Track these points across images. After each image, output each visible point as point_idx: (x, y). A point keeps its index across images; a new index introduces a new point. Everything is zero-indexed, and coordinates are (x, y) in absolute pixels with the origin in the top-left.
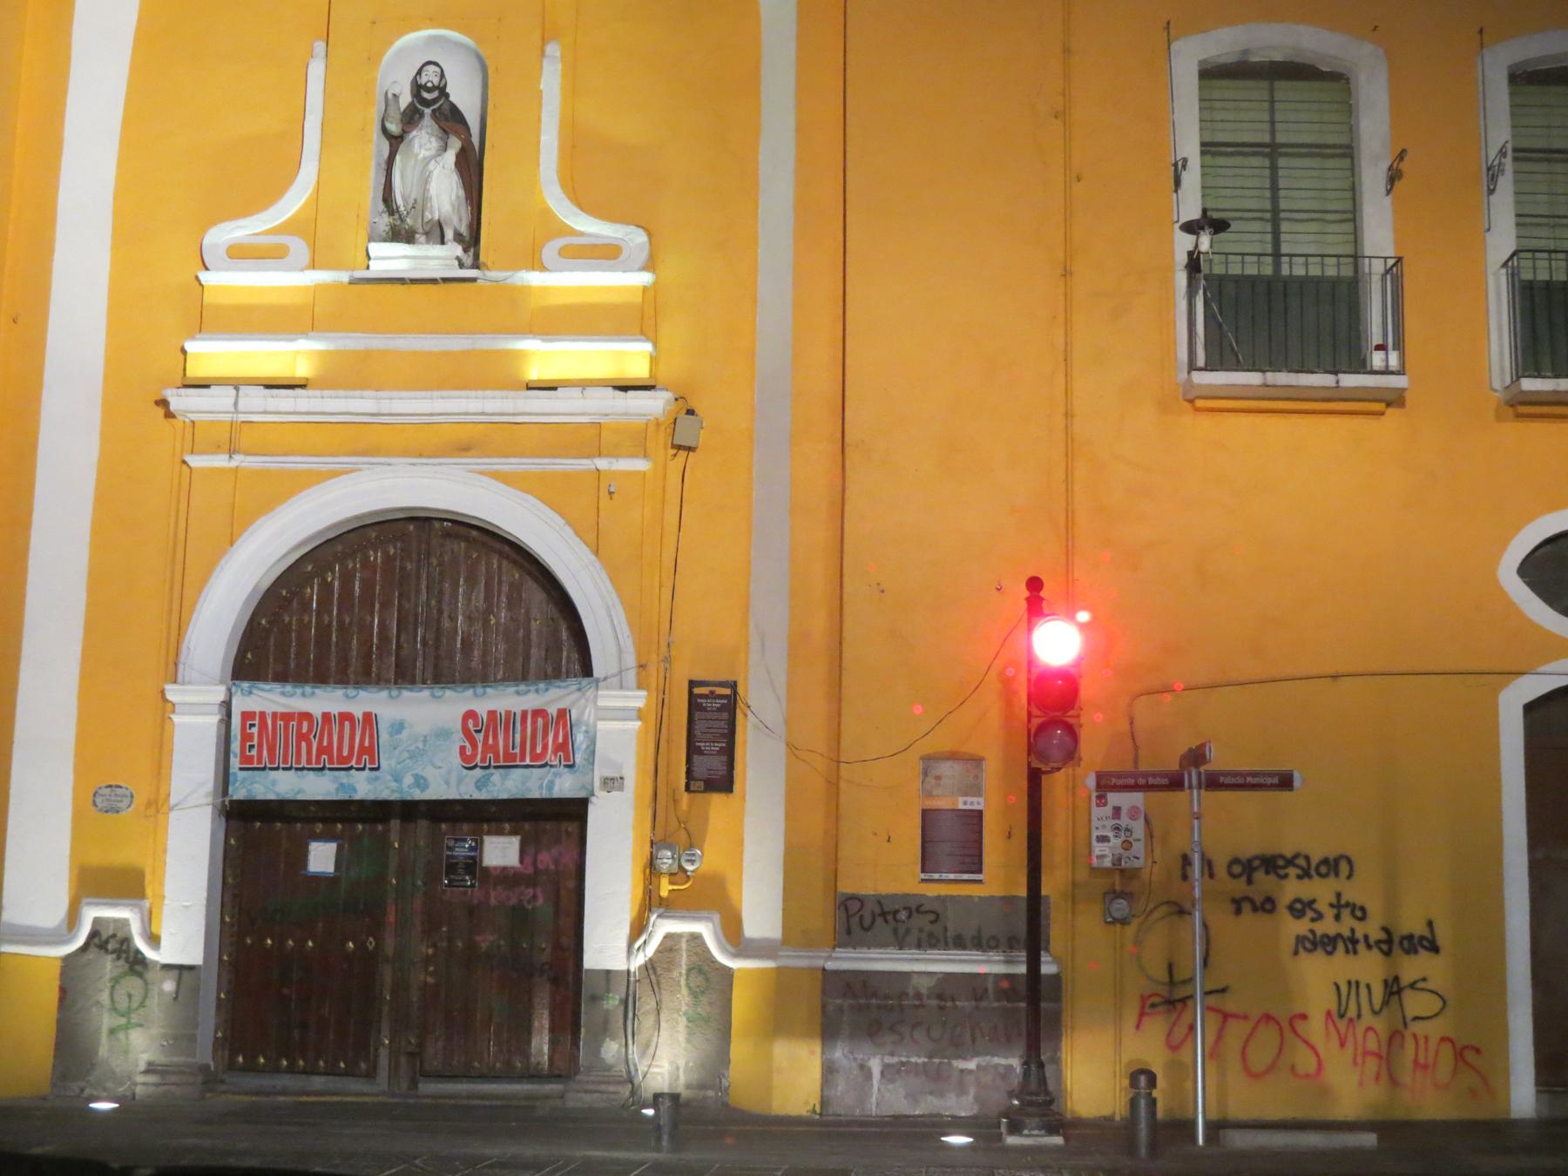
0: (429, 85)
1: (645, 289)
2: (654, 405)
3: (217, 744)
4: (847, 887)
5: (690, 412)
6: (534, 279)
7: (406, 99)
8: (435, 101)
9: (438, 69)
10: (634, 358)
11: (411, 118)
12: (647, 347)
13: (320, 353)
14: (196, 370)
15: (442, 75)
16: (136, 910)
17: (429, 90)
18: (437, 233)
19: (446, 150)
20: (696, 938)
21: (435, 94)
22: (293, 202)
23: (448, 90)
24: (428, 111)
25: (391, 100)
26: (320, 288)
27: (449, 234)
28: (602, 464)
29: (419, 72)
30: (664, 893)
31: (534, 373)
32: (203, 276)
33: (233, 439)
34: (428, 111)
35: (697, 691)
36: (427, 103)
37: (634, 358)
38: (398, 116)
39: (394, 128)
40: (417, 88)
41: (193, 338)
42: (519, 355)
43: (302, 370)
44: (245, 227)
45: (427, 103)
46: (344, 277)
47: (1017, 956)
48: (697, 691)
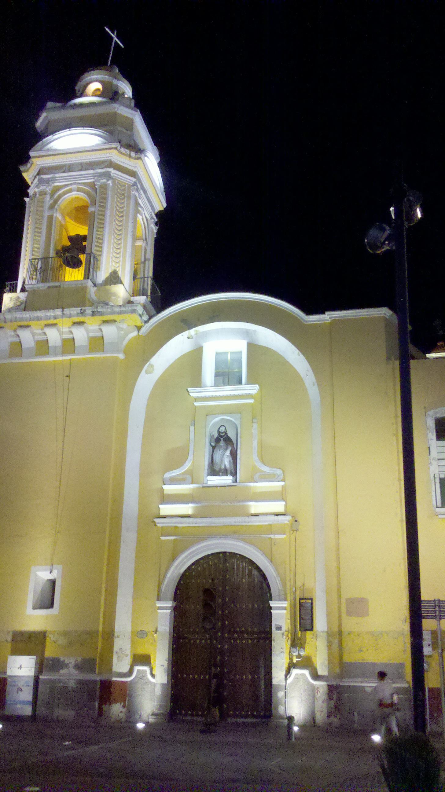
0: (222, 432)
1: (283, 486)
2: (286, 519)
3: (170, 618)
4: (69, 235)
5: (296, 521)
6: (252, 484)
7: (216, 435)
8: (224, 435)
9: (224, 427)
10: (279, 506)
11: (217, 440)
12: (284, 503)
13: (193, 507)
14: (162, 513)
15: (226, 429)
16: (149, 667)
17: (222, 433)
18: (225, 472)
19: (227, 450)
20: (304, 675)
21: (224, 434)
22: (187, 466)
23: (227, 432)
24: (222, 439)
25: (212, 437)
26: (194, 489)
27: (229, 472)
28: (272, 536)
29: (219, 428)
30: (295, 661)
31: (253, 511)
32: (164, 487)
33: (174, 531)
34: (222, 439)
35: (302, 601)
36: (222, 437)
37: (279, 506)
38: (214, 441)
39: (213, 444)
40: (219, 433)
41: (162, 504)
42: (248, 506)
43: (190, 512)
44: (174, 473)
45: (222, 437)
46: (201, 486)
47: (51, 265)
48: (302, 601)
